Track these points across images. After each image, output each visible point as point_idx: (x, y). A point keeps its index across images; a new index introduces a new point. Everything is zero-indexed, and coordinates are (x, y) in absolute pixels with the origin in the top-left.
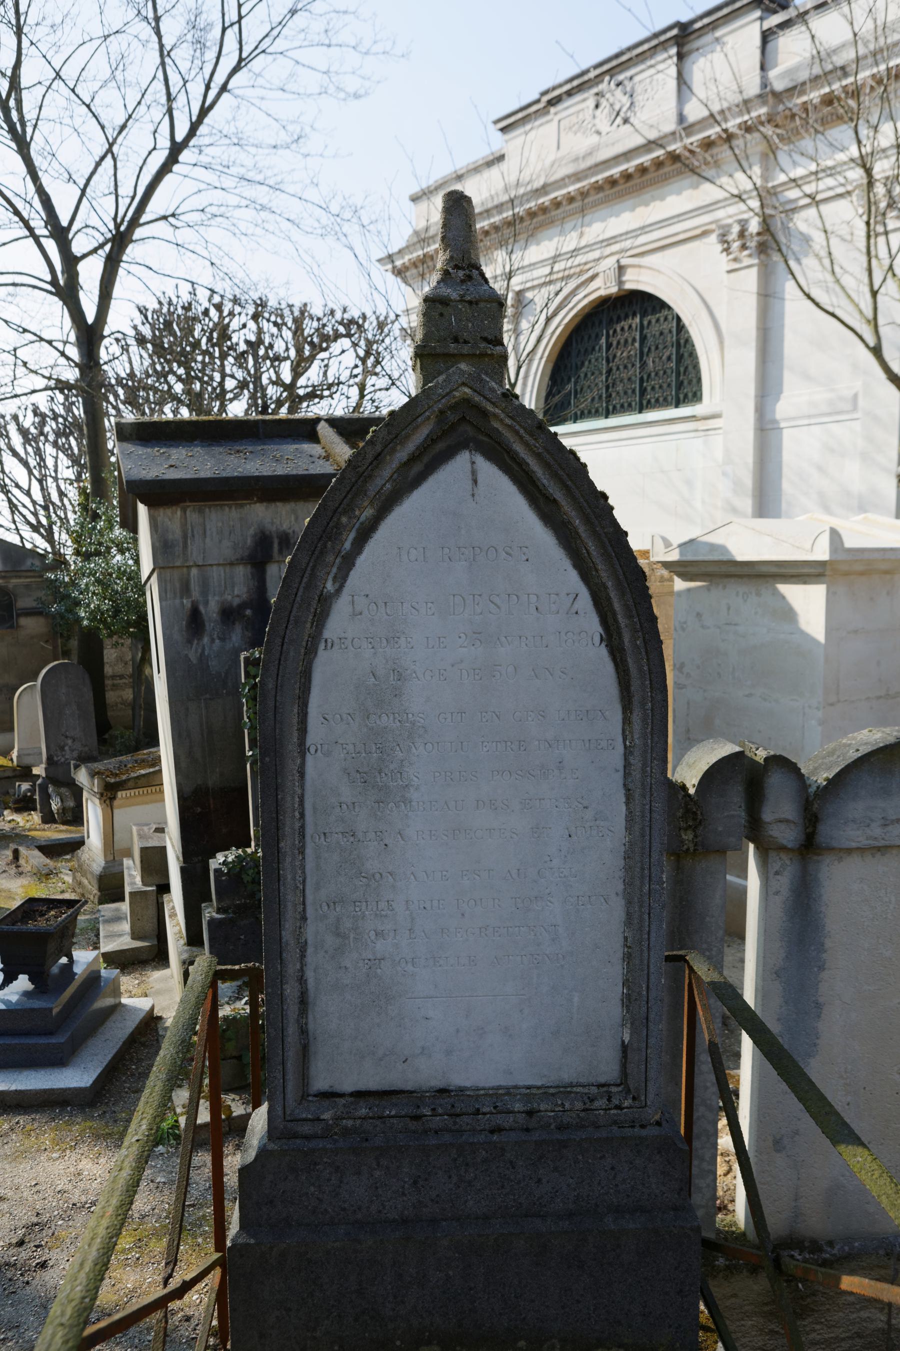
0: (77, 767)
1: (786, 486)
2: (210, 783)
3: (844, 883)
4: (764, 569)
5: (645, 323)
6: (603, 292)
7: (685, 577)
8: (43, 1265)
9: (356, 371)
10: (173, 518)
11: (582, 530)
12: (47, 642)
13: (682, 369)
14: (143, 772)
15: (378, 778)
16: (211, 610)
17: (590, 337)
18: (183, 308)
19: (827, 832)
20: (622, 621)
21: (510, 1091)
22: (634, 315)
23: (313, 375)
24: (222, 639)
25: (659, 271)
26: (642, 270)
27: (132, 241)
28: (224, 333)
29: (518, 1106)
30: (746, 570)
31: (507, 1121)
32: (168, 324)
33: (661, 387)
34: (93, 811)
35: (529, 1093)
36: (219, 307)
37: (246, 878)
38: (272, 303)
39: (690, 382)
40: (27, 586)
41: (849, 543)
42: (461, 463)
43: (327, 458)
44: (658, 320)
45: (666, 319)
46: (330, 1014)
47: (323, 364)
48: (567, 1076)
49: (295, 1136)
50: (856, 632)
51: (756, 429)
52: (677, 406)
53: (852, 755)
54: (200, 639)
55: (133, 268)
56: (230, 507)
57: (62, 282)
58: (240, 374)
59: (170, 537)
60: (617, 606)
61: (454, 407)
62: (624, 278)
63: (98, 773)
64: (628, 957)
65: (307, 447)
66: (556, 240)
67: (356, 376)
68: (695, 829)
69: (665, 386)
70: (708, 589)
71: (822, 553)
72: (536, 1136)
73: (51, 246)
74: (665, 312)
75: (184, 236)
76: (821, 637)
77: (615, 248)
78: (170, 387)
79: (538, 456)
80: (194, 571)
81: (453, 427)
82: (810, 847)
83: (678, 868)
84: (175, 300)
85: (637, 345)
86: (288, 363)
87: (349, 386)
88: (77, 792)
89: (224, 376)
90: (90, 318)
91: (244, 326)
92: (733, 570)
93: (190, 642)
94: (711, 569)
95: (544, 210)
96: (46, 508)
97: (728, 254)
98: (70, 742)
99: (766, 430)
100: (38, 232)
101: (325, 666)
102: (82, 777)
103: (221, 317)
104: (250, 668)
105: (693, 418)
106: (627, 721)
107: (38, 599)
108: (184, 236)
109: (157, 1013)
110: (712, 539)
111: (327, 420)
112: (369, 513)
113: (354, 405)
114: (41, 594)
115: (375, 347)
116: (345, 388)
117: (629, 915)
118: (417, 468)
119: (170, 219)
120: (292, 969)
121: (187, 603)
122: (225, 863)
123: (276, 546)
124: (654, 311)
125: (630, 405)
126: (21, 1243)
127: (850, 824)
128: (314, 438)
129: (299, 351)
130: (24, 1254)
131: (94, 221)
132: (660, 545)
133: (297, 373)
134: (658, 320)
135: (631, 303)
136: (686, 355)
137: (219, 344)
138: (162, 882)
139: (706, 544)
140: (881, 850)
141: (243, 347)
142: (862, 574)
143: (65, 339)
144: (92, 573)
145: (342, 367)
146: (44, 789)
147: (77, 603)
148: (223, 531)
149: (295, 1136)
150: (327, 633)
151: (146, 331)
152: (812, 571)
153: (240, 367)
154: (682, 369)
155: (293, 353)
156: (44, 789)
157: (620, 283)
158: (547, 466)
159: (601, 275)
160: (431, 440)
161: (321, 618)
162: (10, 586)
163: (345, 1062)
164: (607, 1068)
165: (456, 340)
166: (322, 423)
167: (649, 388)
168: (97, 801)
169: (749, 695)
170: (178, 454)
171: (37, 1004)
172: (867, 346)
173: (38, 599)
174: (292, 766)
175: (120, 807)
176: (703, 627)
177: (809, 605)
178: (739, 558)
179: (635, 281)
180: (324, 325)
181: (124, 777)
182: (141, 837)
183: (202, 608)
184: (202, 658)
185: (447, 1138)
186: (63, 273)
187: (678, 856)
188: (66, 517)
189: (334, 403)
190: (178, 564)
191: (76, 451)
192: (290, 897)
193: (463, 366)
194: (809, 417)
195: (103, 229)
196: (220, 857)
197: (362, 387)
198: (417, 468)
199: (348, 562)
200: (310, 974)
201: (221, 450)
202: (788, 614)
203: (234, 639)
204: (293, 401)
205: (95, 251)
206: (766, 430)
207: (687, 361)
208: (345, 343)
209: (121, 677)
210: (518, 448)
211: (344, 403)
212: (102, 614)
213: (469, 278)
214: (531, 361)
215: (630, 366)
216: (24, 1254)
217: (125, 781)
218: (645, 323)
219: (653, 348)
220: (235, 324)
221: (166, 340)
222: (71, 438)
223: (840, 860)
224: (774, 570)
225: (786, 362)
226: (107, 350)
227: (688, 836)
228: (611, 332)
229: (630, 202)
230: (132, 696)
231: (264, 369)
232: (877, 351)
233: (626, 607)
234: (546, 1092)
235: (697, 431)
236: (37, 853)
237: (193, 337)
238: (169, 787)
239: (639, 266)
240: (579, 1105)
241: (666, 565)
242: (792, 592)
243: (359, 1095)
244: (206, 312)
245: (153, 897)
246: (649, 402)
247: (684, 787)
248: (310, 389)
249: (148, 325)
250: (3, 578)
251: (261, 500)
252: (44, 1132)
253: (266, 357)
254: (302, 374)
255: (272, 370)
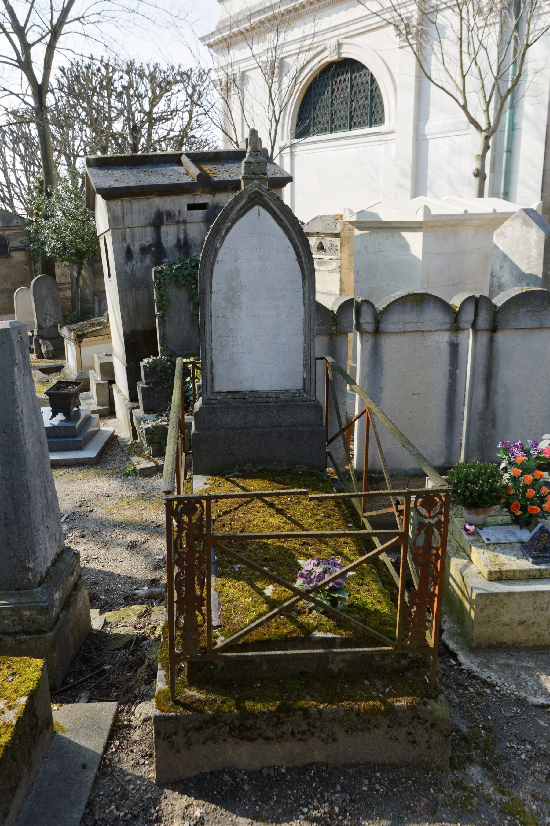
0: (61, 327)
1: (430, 172)
2: (138, 328)
3: (390, 345)
4: (395, 225)
5: (353, 77)
6: (329, 59)
7: (360, 228)
8: (92, 511)
9: (187, 103)
10: (117, 205)
11: (290, 228)
12: (26, 265)
13: (374, 105)
14: (94, 329)
15: (232, 301)
16: (136, 249)
17: (322, 85)
18: (86, 67)
19: (384, 326)
20: (302, 254)
21: (271, 392)
22: (347, 72)
23: (161, 106)
24: (142, 262)
25: (361, 47)
26: (352, 46)
27: (61, 35)
28: (110, 81)
29: (273, 396)
30: (387, 225)
31: (271, 400)
32: (77, 78)
33: (362, 115)
34: (70, 349)
35: (277, 392)
36: (107, 66)
37: (158, 369)
38: (137, 65)
39: (378, 112)
40: (15, 235)
41: (433, 213)
42: (256, 209)
43: (187, 174)
44: (360, 76)
45: (365, 75)
46: (219, 369)
47: (167, 99)
48: (287, 387)
49: (210, 404)
50: (437, 254)
51: (414, 140)
52: (370, 127)
53: (393, 299)
54: (131, 262)
55: (59, 50)
56: (143, 199)
57: (22, 59)
58: (119, 105)
59: (117, 214)
60: (300, 250)
61: (253, 193)
62: (341, 51)
63: (73, 330)
64: (305, 352)
65: (177, 168)
66: (302, 27)
67: (187, 106)
68: (336, 325)
69: (364, 114)
70: (370, 234)
71: (420, 218)
72: (279, 404)
73: (15, 38)
74: (364, 71)
75: (89, 29)
76: (420, 257)
77: (337, 32)
78: (79, 115)
79: (277, 207)
80: (128, 230)
81: (253, 199)
82: (377, 332)
83: (331, 339)
84: (81, 63)
85: (348, 90)
86: (148, 98)
87: (183, 112)
88: (61, 339)
89: (110, 107)
90: (40, 80)
91: (121, 77)
92: (381, 225)
93: (127, 263)
94: (371, 225)
95: (295, 9)
96: (8, 187)
97: (400, 37)
98: (49, 317)
99: (419, 140)
100: (8, 30)
101: (217, 268)
102: (64, 332)
103: (108, 72)
104: (158, 276)
105: (379, 133)
106: (304, 283)
107: (21, 242)
108: (89, 29)
109: (115, 434)
110: (371, 210)
111: (186, 154)
112: (229, 224)
113: (186, 123)
114: (23, 239)
115: (198, 88)
116: (181, 114)
117: (305, 340)
118: (243, 211)
119: (82, 20)
120: (208, 356)
121: (125, 245)
122: (148, 363)
123: (165, 218)
124: (358, 70)
125: (344, 126)
126: (80, 506)
127: (391, 323)
128: (179, 163)
129: (154, 92)
130: (82, 509)
131: (38, 22)
132: (347, 212)
133: (153, 104)
134: (360, 76)
135: (345, 65)
136: (376, 96)
137: (107, 88)
138: (111, 379)
139: (369, 212)
140: (404, 332)
141: (120, 89)
142: (441, 227)
143: (24, 92)
144: (51, 227)
145: (179, 100)
146: (37, 341)
147: (43, 244)
148: (141, 210)
149: (210, 404)
150: (217, 259)
151: (64, 81)
152: (416, 226)
153: (119, 101)
154: (374, 105)
155: (150, 94)
156: (37, 341)
157: (339, 54)
158: (280, 210)
159: (328, 49)
160: (247, 203)
161: (216, 254)
162: (6, 235)
163: (223, 384)
164: (300, 386)
165: (254, 174)
166: (184, 156)
167: (355, 116)
168: (73, 344)
169: (389, 285)
170: (117, 173)
171: (68, 424)
172: (459, 104)
173: (21, 242)
174: (208, 297)
175: (84, 346)
176: (368, 253)
177: (415, 241)
178: (384, 220)
179: (348, 53)
180: (168, 76)
181: (86, 332)
182: (99, 358)
183: (132, 248)
184: (132, 270)
185: (253, 404)
186: (22, 54)
187: (331, 335)
188: (21, 193)
189: (174, 122)
190: (120, 227)
191: (23, 152)
192: (208, 335)
193: (256, 181)
194: (443, 132)
195: (44, 26)
196: (146, 360)
197: (190, 113)
198: (243, 211)
199: (223, 238)
200: (213, 358)
201: (137, 170)
202: (406, 246)
203: (147, 261)
204: (150, 122)
205: (40, 40)
206: (419, 140)
207: (376, 100)
208: (180, 86)
209: (64, 284)
210: (272, 205)
211: (180, 122)
212: (57, 249)
213: (257, 155)
214: (286, 110)
215: (344, 103)
216: (82, 509)
217: (86, 334)
218: (353, 77)
219: (357, 92)
220: (116, 76)
221: (76, 87)
222: (20, 145)
223: (389, 337)
224: (400, 225)
225: (432, 101)
226: (50, 100)
227: (334, 328)
228: (334, 83)
229: (344, 6)
230: (71, 294)
231: (133, 102)
232: (464, 107)
233: (303, 250)
234: (282, 392)
235: (381, 141)
236: (39, 372)
237: (92, 85)
238: (117, 333)
239: (350, 44)
240: (291, 395)
241: (351, 223)
242: (407, 236)
243: (228, 392)
244: (99, 70)
245: (107, 386)
246: (355, 124)
247: (333, 311)
248: (159, 115)
249: (65, 78)
250: (2, 230)
251: (158, 196)
252: (79, 474)
253: (135, 95)
254: (155, 105)
255: (137, 103)
